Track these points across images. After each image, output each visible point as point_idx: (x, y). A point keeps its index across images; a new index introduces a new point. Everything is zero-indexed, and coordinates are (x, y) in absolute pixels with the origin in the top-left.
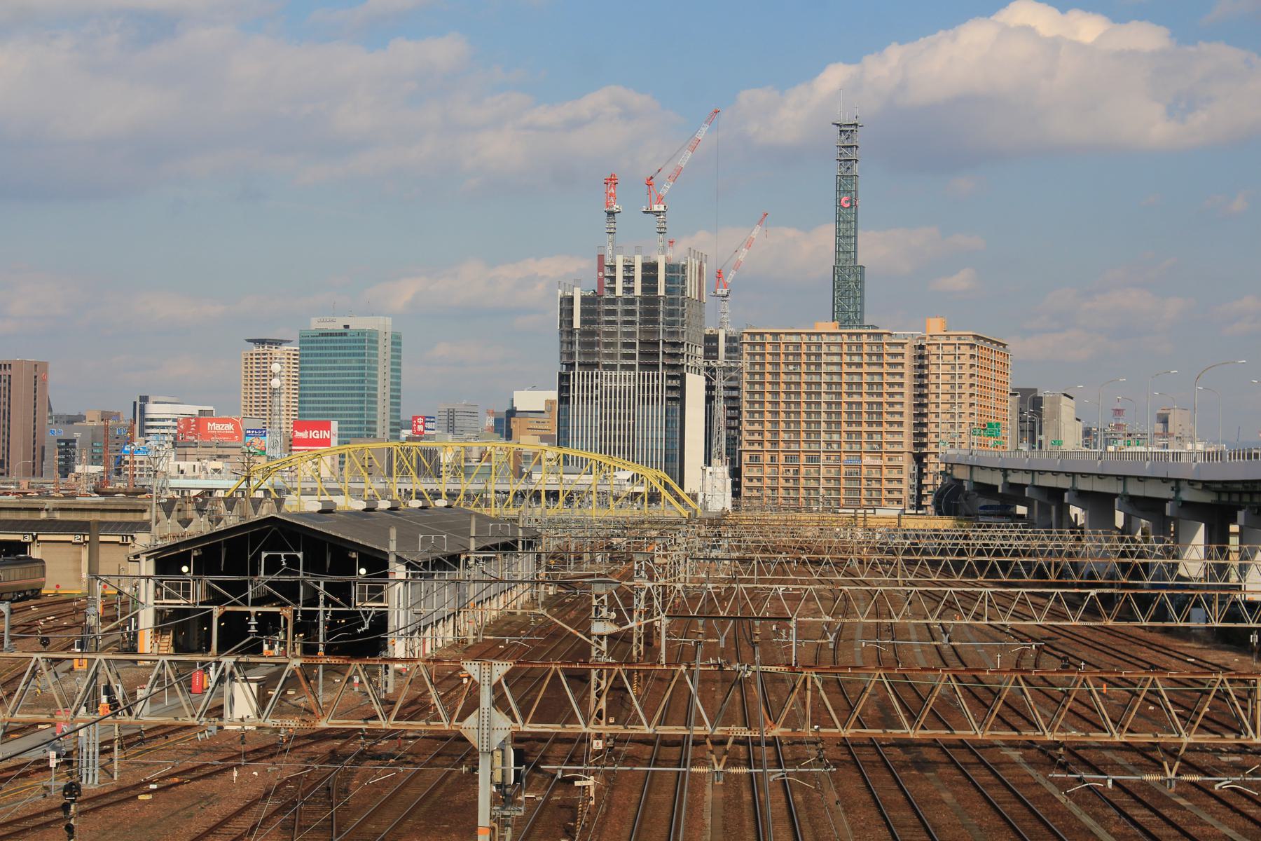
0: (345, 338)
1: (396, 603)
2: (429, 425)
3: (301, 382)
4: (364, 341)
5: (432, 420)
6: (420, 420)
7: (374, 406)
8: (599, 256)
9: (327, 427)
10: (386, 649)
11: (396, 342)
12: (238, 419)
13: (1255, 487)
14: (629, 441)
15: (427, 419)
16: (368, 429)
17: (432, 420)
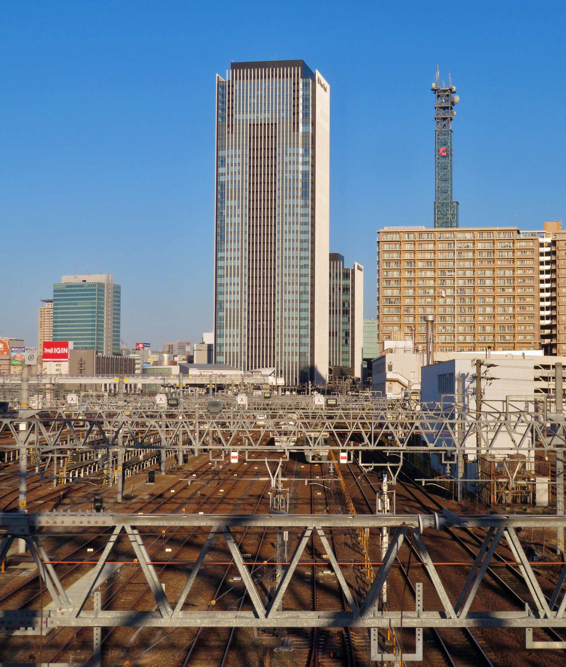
1: (386, 229)
4: (95, 290)
9: (65, 345)
10: (184, 376)
11: (117, 291)
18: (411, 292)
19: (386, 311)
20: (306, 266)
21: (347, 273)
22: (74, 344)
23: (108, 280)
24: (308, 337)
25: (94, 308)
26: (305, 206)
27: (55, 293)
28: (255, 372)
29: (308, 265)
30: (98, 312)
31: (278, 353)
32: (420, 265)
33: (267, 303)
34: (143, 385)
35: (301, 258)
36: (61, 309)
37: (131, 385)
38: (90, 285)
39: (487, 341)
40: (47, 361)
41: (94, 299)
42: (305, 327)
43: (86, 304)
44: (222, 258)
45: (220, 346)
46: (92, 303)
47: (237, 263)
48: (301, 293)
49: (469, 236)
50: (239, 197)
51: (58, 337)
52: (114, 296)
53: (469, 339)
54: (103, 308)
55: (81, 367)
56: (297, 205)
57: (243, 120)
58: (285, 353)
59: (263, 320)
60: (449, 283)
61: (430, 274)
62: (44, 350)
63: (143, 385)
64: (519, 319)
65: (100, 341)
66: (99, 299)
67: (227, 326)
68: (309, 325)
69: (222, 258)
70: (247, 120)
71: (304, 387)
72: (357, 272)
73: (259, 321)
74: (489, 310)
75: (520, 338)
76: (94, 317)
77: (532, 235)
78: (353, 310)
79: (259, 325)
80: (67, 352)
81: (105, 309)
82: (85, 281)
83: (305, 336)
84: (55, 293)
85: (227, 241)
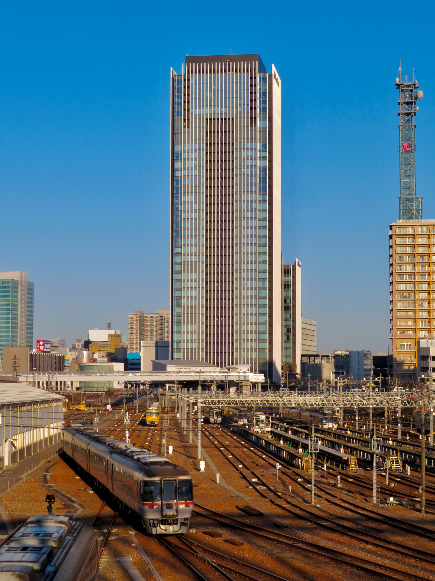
2: (47, 346)
5: (49, 343)
7: (16, 290)
11: (30, 288)
13: (333, 570)
14: (240, 99)
15: (46, 342)
16: (13, 309)
17: (49, 343)
57: (199, 114)
70: (203, 114)
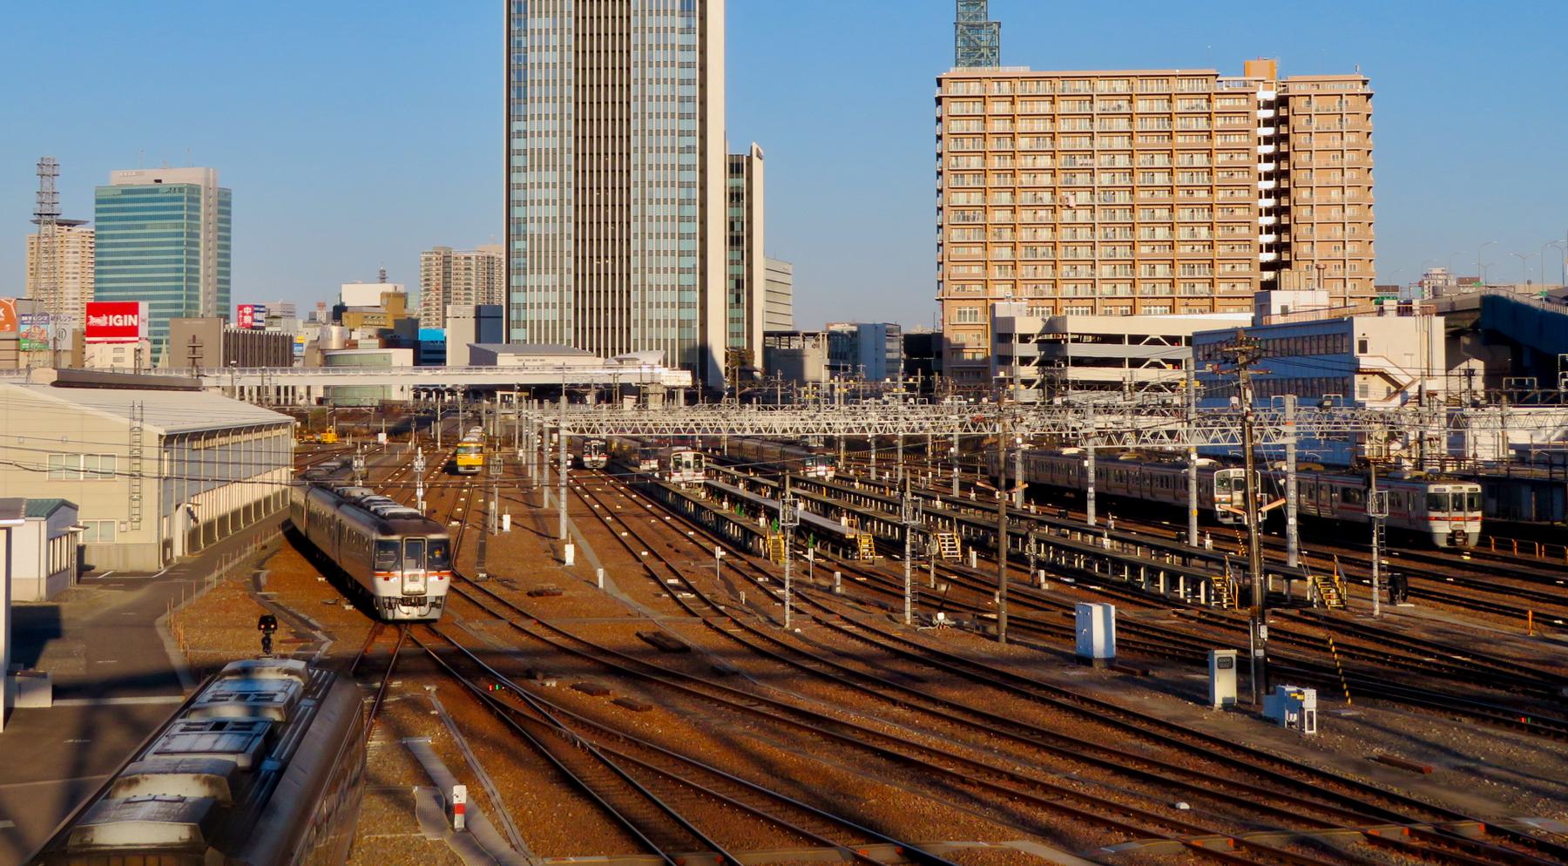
0: (157, 195)
3: (98, 237)
4: (181, 199)
6: (248, 310)
8: (381, 271)
9: (132, 309)
11: (224, 203)
12: (10, 301)
15: (256, 309)
18: (1005, 198)
19: (956, 235)
20: (690, 149)
21: (738, 165)
22: (151, 306)
23: (207, 179)
24: (695, 290)
25: (181, 234)
26: (688, 30)
27: (99, 206)
28: (627, 359)
29: (695, 147)
30: (189, 244)
31: (636, 321)
32: (1023, 143)
33: (613, 223)
34: (326, 388)
35: (681, 134)
36: (112, 237)
37: (286, 388)
38: (172, 189)
39: (1158, 295)
40: (95, 342)
41: (181, 217)
42: (689, 271)
43: (164, 227)
44: (523, 134)
45: (519, 309)
46: (176, 226)
47: (554, 143)
48: (681, 203)
49: (1121, 87)
50: (555, 12)
51: (104, 294)
52: (220, 212)
53: (1123, 290)
54: (197, 236)
55: (194, 352)
56: (673, 29)
58: (651, 321)
59: (606, 257)
60: (1082, 179)
61: (1044, 162)
62: (88, 320)
63: (326, 388)
64: (1221, 250)
65: (192, 302)
66: (189, 217)
67: (532, 268)
68: (698, 266)
69: (523, 134)
71: (792, 388)
72: (756, 161)
73: (599, 257)
74: (1162, 233)
75: (1222, 288)
76: (181, 252)
77: (1245, 86)
78: (750, 235)
79: (599, 266)
80: (135, 324)
81: (202, 236)
82: (159, 181)
83: (690, 288)
84: (99, 206)
85: (532, 98)
